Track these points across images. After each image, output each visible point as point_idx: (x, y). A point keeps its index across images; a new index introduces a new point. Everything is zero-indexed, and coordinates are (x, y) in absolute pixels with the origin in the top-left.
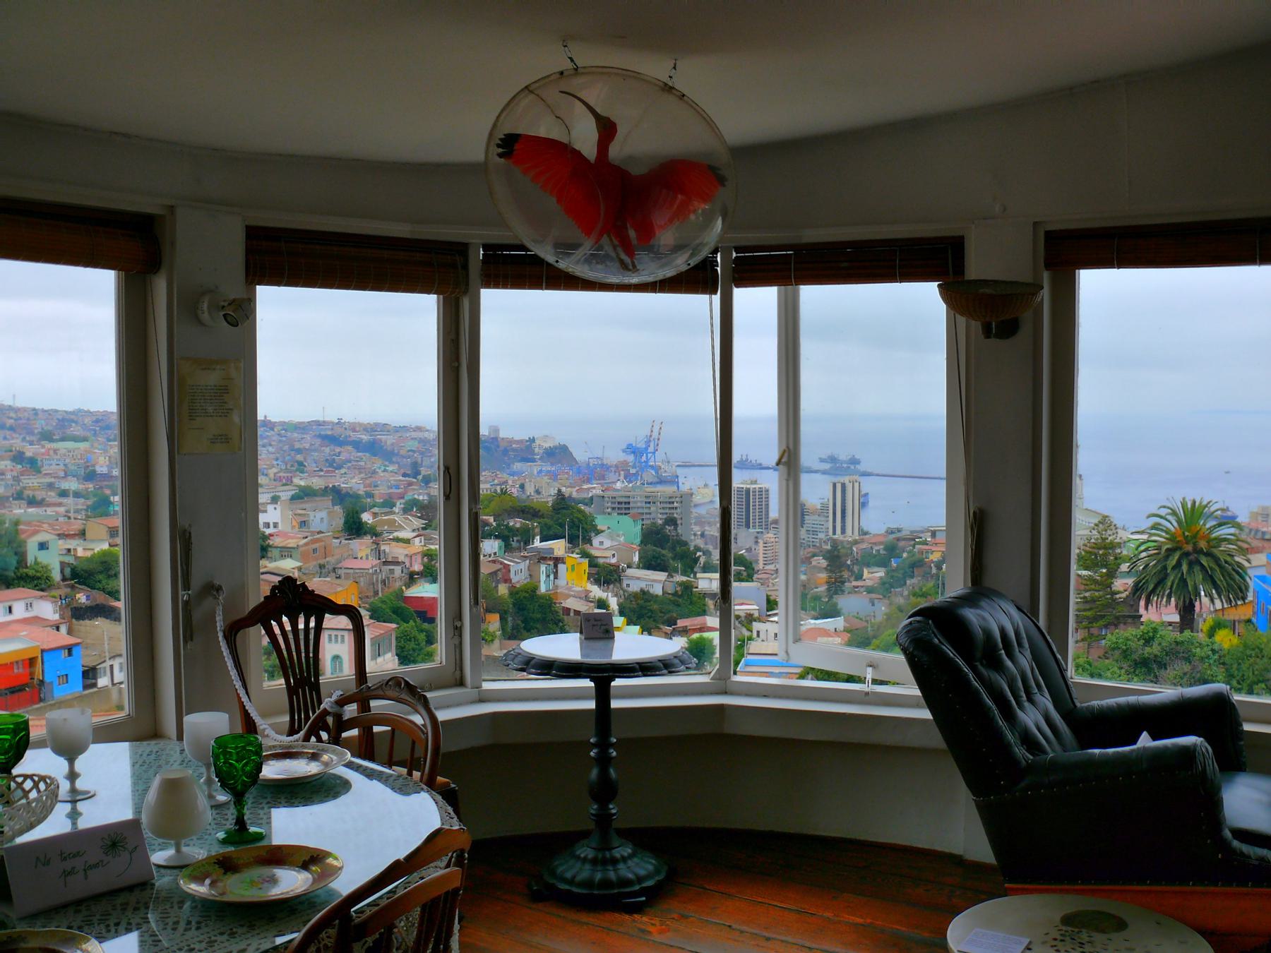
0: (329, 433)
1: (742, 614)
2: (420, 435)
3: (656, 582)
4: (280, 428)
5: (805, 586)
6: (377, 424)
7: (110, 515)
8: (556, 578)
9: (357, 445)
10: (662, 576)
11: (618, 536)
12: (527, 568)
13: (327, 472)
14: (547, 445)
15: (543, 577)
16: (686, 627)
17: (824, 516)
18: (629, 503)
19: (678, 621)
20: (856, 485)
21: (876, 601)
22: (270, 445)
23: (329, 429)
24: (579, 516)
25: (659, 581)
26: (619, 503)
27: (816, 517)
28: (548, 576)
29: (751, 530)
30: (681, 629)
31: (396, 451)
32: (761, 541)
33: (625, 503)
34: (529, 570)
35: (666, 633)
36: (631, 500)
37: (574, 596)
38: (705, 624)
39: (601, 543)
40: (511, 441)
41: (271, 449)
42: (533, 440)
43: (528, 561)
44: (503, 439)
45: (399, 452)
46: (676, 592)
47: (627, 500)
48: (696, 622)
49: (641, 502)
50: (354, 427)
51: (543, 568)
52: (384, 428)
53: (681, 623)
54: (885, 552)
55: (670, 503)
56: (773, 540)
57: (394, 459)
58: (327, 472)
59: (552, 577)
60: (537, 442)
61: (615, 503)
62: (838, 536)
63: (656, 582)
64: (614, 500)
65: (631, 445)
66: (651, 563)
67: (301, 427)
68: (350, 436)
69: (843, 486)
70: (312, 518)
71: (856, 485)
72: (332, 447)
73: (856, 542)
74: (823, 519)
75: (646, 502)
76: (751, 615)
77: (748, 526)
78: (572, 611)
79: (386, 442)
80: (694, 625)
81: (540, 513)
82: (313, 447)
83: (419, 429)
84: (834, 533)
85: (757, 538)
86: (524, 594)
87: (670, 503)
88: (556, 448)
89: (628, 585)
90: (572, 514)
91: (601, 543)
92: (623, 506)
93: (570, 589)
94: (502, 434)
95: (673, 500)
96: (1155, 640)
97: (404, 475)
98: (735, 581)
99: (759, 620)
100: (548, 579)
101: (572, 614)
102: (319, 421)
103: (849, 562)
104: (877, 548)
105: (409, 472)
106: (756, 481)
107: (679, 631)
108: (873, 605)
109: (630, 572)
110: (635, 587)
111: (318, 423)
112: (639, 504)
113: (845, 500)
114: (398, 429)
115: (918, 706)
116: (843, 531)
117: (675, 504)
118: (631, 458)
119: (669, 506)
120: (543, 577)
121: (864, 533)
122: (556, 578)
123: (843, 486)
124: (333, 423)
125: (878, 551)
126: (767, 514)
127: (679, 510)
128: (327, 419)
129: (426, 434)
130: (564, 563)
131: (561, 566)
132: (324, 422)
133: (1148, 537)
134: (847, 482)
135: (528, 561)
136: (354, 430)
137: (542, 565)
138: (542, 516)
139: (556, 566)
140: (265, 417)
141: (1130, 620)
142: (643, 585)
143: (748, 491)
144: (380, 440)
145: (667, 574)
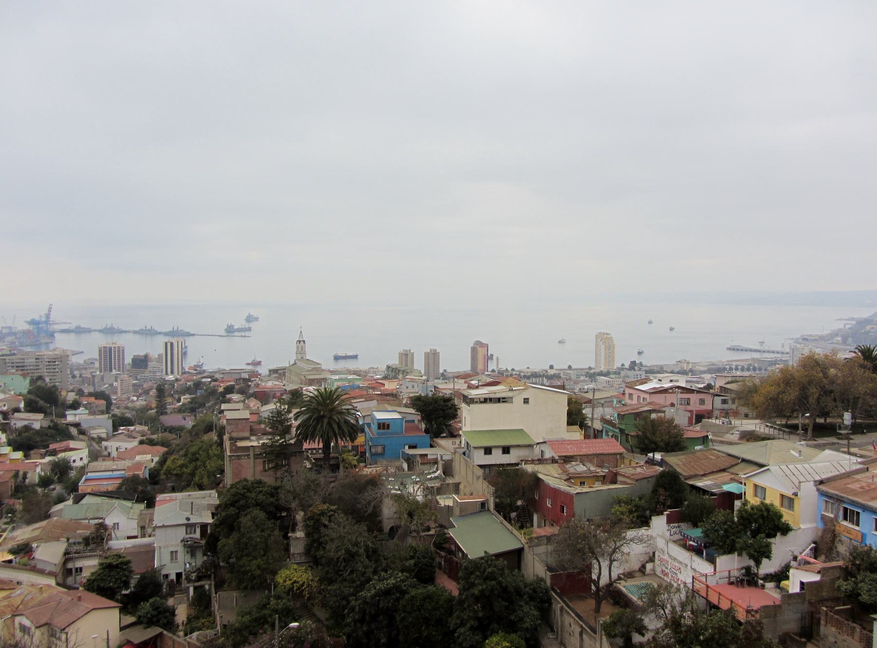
1: (95, 436)
3: (37, 421)
10: (40, 416)
11: (10, 390)
16: (56, 449)
19: (50, 445)
21: (187, 418)
26: (12, 363)
33: (53, 362)
35: (41, 454)
36: (26, 361)
38: (69, 446)
48: (62, 445)
55: (53, 362)
63: (37, 421)
64: (13, 365)
66: (32, 407)
77: (111, 370)
80: (61, 447)
84: (167, 374)
85: (116, 377)
89: (15, 424)
92: (51, 364)
96: (272, 521)
98: (66, 420)
99: (106, 440)
108: (185, 419)
115: (235, 475)
117: (57, 363)
118: (31, 328)
119: (35, 368)
123: (172, 344)
127: (59, 367)
141: (298, 454)
142: (26, 423)
143: (110, 348)
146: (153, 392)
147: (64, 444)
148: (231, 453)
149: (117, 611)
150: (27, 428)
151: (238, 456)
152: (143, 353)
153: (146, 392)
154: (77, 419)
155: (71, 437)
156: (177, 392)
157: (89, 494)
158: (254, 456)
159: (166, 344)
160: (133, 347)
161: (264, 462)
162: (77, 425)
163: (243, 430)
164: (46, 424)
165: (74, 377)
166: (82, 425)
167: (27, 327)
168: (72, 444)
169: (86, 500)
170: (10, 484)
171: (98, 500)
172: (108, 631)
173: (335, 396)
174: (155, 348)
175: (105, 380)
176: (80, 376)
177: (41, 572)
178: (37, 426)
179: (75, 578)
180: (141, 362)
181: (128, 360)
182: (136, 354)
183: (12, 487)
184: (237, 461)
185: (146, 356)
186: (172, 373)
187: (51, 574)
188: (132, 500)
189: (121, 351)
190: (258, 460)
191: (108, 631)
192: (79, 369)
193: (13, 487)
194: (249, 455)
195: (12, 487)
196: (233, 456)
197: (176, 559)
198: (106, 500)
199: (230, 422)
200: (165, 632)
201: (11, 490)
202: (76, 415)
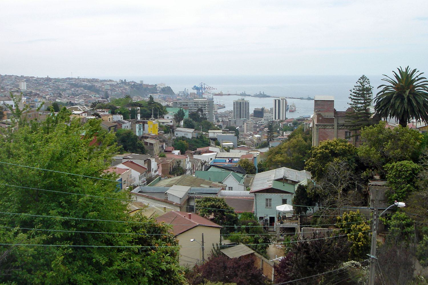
0: (74, 82)
2: (111, 83)
3: (189, 133)
4: (54, 81)
5: (260, 139)
6: (93, 79)
7: (419, 262)
8: (144, 130)
9: (85, 87)
10: (192, 130)
12: (130, 126)
13: (71, 97)
14: (162, 87)
15: (137, 130)
17: (272, 113)
18: (187, 105)
19: (197, 149)
20: (284, 101)
22: (50, 87)
23: (74, 81)
24: (158, 106)
25: (190, 132)
27: (268, 114)
28: (140, 129)
29: (241, 119)
30: (198, 152)
31: (101, 90)
32: (245, 124)
34: (131, 127)
36: (188, 104)
37: (151, 137)
39: (168, 118)
40: (148, 85)
41: (50, 89)
42: (156, 85)
43: (130, 123)
44: (144, 84)
45: (102, 90)
46: (197, 137)
47: (186, 104)
48: (204, 149)
49: (193, 105)
50: (84, 80)
51: (137, 125)
52: (96, 81)
53: (198, 150)
54: (293, 125)
56: (250, 122)
57: (100, 93)
58: (71, 97)
59: (142, 130)
60: (158, 86)
61: (181, 105)
62: (274, 120)
63: (189, 133)
64: (181, 104)
65: (195, 86)
67: (64, 80)
68: (82, 84)
69: (279, 101)
70: (37, 105)
71: (284, 101)
72: (75, 88)
73: (282, 121)
74: (271, 114)
75: (194, 105)
76: (230, 147)
78: (149, 144)
79: (97, 86)
81: (142, 106)
82: (67, 88)
83: (111, 81)
84: (275, 119)
86: (125, 135)
87: (204, 105)
88: (165, 88)
89: (177, 134)
90: (155, 105)
91: (168, 118)
93: (149, 134)
94: (144, 83)
95: (206, 104)
97: (102, 98)
99: (233, 149)
100: (140, 131)
101: (149, 145)
102: (70, 78)
103: (278, 130)
104: (290, 124)
105: (104, 97)
106: (244, 99)
107: (197, 153)
109: (178, 129)
110: (180, 135)
111: (69, 79)
112: (191, 106)
113: (280, 104)
114: (101, 81)
116: (279, 118)
118: (195, 91)
120: (137, 130)
121: (286, 119)
122: (144, 130)
123: (279, 101)
124: (75, 79)
125: (290, 125)
126: (248, 113)
128: (73, 77)
129: (113, 83)
130: (147, 124)
131: (145, 125)
132: (72, 78)
133: (383, 93)
134: (280, 99)
135: (130, 123)
136: (84, 81)
137: (137, 124)
138: (143, 107)
139: (144, 125)
140: (48, 76)
143: (240, 103)
144: (95, 85)
145: (194, 130)
146: (266, 129)
147: (205, 149)
148: (317, 123)
149: (218, 232)
150: (183, 138)
151: (325, 125)
152: (260, 107)
153: (262, 130)
154: (215, 136)
155: (209, 145)
156: (281, 129)
157: (213, 166)
158: (338, 126)
159: (275, 100)
160: (254, 105)
161: (346, 132)
162: (214, 139)
163: (328, 111)
164: (195, 135)
165: (218, 121)
166: (218, 139)
167: (191, 91)
168: (210, 149)
169: (212, 169)
170: (169, 165)
171: (219, 170)
172: (203, 234)
173: (406, 110)
174: (268, 104)
175: (237, 123)
176: (222, 121)
177: (171, 203)
178: (190, 136)
179: (141, 122)
180: (259, 113)
181: (251, 112)
182: (256, 108)
183: (170, 168)
184: (323, 130)
185: (263, 109)
186: (279, 118)
187: (176, 205)
188: (242, 173)
189: (247, 104)
190: (341, 131)
191: (203, 234)
192: (221, 116)
193: (172, 168)
194: (333, 125)
195: (170, 168)
196: (320, 125)
197: (270, 206)
198: (224, 171)
199: (318, 103)
200: (256, 254)
201: (170, 169)
202: (214, 133)
